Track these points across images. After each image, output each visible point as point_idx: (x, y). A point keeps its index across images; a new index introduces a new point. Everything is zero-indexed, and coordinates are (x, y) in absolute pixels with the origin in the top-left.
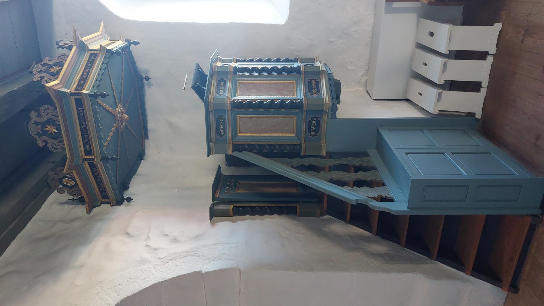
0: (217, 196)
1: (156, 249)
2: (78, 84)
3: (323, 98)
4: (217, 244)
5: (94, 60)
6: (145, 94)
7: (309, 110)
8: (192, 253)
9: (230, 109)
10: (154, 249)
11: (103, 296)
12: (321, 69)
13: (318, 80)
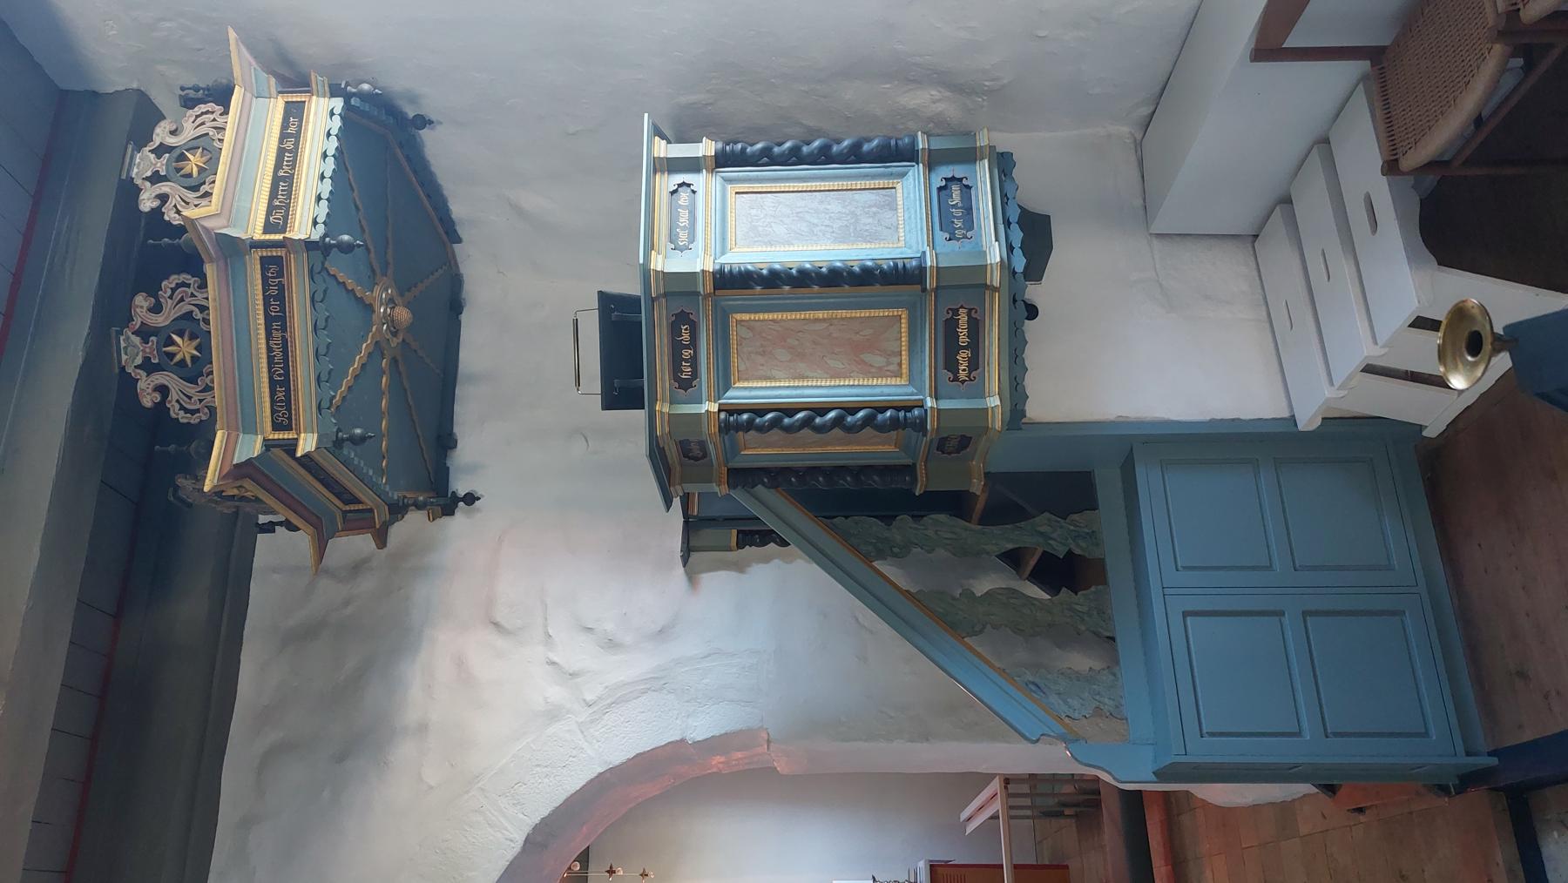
0: (693, 511)
1: (573, 675)
2: (273, 402)
3: (984, 249)
4: (709, 655)
5: (281, 287)
6: (422, 141)
7: (944, 287)
8: (655, 683)
9: (712, 291)
10: (570, 675)
11: (493, 818)
12: (991, 281)
13: (976, 312)
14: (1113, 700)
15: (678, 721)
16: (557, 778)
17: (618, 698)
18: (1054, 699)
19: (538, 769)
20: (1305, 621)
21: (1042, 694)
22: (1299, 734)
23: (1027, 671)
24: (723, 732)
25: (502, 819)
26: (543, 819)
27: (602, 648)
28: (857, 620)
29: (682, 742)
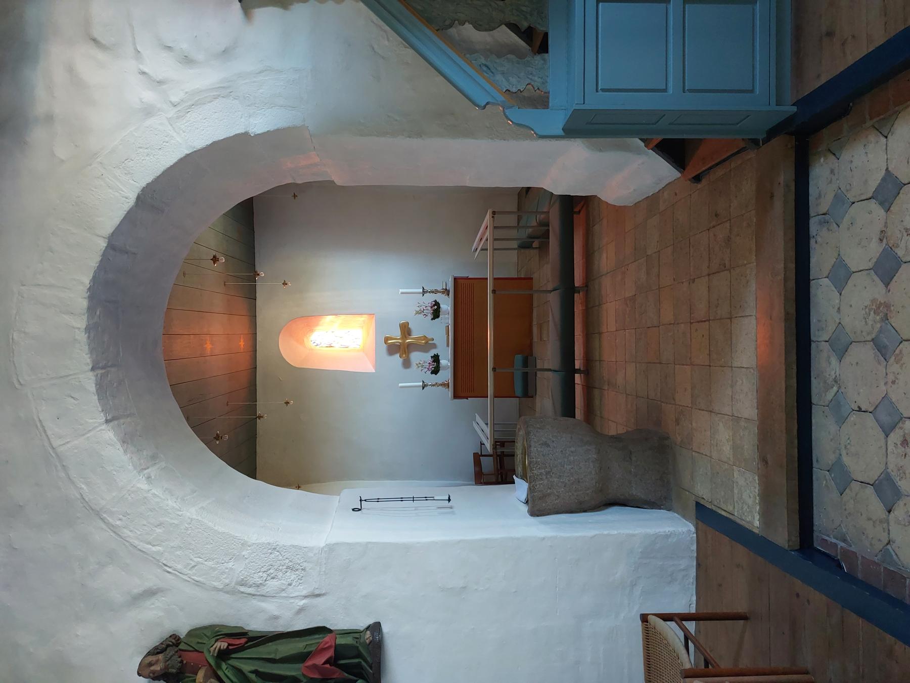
1: (160, 82)
8: (224, 91)
14: (541, 78)
15: (242, 120)
16: (155, 156)
17: (196, 101)
18: (499, 77)
19: (141, 150)
20: (684, 8)
21: (491, 73)
22: (665, 90)
23: (481, 57)
24: (276, 128)
25: (119, 184)
26: (148, 184)
27: (180, 63)
28: (373, 48)
29: (246, 134)
